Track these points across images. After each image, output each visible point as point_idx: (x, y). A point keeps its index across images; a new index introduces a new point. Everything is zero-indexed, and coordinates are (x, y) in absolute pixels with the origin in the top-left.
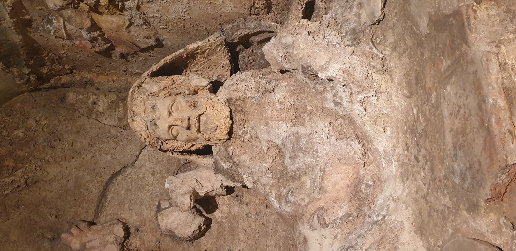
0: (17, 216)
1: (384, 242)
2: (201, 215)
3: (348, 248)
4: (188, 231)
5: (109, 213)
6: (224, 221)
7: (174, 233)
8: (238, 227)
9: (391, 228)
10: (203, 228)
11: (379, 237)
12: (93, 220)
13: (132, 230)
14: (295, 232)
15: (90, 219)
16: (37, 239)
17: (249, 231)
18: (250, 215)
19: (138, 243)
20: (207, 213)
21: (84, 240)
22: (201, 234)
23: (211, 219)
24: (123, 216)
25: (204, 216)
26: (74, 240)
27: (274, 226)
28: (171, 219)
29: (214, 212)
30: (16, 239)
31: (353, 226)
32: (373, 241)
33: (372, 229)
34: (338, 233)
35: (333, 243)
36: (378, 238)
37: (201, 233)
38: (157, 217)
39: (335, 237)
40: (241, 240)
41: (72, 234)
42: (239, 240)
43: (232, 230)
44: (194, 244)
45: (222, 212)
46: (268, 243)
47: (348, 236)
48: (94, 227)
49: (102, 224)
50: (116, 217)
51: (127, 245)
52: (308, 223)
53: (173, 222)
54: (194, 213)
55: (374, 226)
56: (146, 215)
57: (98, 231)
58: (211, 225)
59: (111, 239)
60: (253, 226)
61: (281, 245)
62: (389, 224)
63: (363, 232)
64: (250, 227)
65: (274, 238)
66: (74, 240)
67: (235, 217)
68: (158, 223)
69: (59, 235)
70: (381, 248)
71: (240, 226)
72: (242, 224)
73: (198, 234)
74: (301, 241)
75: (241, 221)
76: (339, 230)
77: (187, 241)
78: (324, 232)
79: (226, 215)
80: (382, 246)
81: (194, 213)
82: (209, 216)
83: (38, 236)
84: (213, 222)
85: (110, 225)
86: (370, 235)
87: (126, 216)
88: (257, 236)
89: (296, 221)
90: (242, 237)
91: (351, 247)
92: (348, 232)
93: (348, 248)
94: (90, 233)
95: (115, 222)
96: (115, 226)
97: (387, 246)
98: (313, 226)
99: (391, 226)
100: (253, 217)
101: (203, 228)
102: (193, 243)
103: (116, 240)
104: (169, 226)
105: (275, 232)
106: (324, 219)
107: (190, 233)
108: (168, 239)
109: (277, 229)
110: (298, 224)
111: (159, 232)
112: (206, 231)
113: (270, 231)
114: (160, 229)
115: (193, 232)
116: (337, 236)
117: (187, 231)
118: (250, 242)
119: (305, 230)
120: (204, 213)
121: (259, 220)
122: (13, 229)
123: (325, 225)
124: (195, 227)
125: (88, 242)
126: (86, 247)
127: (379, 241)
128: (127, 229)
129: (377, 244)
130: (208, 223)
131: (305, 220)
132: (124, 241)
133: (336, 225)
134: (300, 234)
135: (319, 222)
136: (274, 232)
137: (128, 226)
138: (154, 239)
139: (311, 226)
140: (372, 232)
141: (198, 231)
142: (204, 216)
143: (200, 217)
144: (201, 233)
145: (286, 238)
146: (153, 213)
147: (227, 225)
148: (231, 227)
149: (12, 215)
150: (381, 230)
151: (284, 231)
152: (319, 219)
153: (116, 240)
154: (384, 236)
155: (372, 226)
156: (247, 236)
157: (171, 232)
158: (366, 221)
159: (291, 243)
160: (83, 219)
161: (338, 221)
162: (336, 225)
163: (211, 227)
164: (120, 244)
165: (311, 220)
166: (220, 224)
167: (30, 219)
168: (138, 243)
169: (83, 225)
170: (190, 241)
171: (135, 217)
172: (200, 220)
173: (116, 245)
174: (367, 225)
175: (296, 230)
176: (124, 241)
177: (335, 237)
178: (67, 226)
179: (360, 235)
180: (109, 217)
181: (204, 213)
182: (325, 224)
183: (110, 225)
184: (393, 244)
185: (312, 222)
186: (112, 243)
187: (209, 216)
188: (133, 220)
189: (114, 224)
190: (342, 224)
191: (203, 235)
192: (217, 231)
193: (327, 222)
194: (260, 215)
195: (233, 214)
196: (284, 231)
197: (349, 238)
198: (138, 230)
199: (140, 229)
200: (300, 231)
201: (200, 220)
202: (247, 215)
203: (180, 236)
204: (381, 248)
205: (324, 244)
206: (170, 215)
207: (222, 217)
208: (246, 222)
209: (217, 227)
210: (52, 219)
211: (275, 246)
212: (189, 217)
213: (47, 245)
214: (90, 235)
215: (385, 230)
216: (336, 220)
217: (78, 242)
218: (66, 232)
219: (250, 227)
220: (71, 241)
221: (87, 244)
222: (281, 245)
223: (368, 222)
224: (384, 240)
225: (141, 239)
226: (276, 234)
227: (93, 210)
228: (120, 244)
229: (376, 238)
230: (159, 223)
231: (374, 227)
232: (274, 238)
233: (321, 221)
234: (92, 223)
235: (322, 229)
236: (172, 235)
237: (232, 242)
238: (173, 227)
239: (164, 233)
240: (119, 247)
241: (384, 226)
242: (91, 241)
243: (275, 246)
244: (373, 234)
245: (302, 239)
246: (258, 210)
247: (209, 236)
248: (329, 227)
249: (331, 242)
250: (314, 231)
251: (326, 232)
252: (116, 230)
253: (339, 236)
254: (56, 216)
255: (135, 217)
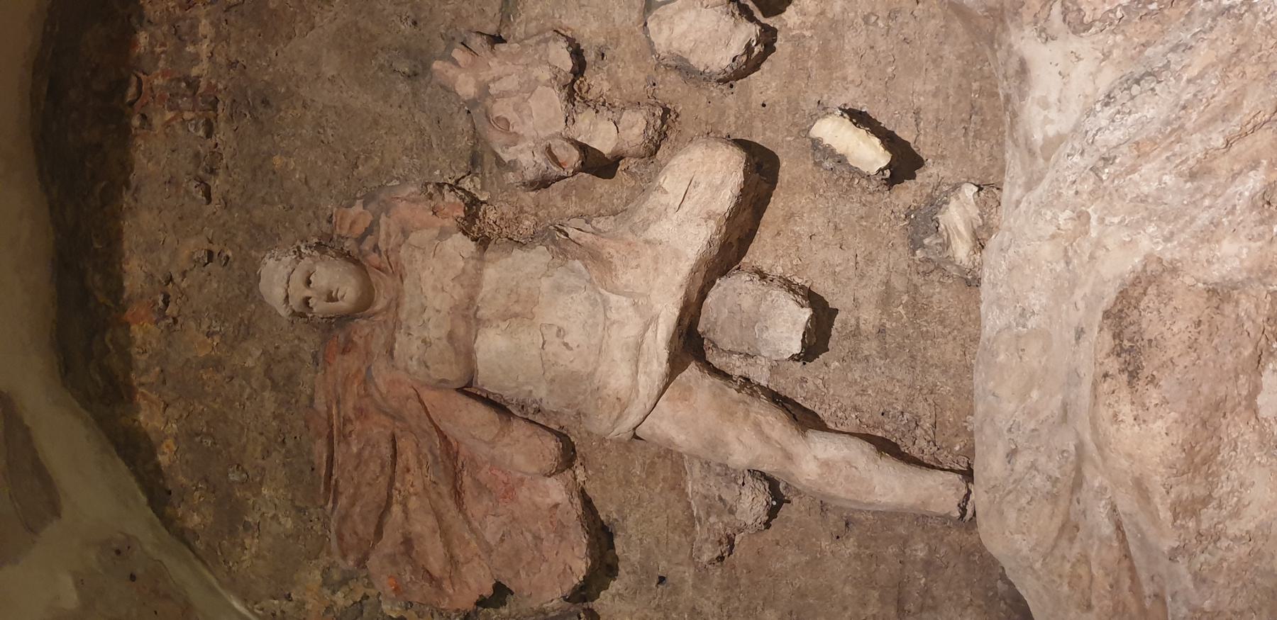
0: (330, 22)
1: (1242, 60)
2: (751, 18)
3: (1142, 77)
4: (722, 58)
5: (533, 15)
6: (808, 34)
7: (687, 61)
8: (843, 48)
9: (1269, 22)
10: (756, 50)
11: (1231, 49)
12: (499, 31)
13: (590, 57)
14: (994, 51)
15: (491, 29)
16: (381, 74)
17: (869, 58)
18: (873, 19)
19: (606, 86)
20: (765, 16)
21: (485, 76)
22: (751, 64)
23: (773, 32)
24: (565, 22)
25: (758, 22)
26: (462, 77)
27: (936, 46)
28: (681, 27)
29: (783, 11)
30: (335, 73)
31: (1157, 27)
32: (1212, 58)
33: (1211, 28)
34: (1115, 45)
35: (1100, 70)
36: (1227, 49)
37: (750, 63)
38: (646, 24)
39: (1106, 56)
40: (849, 79)
41: (455, 62)
42: (845, 79)
43: (828, 58)
44: (736, 89)
45: (803, 13)
46: (918, 86)
47: (1141, 52)
48: (502, 48)
49: (520, 41)
50: (549, 25)
51: (580, 89)
52: (1036, 24)
53: (684, 35)
54: (733, 15)
55: (1221, 20)
56: (618, 21)
57: (513, 57)
58: (776, 45)
59: (545, 74)
60: (882, 45)
61: (951, 92)
62: (1265, 14)
63: (1186, 37)
64: (872, 48)
65: (933, 74)
66: (462, 77)
67: (834, 25)
68: (649, 39)
69: (427, 67)
70: (1231, 75)
71: (847, 47)
72: (854, 40)
73: (746, 63)
74: (1011, 72)
75: (850, 35)
76: (1119, 38)
77: (719, 81)
78: (1075, 44)
79: (812, 19)
80: (1237, 70)
81: (733, 15)
82: (771, 22)
83: (381, 67)
84: (779, 36)
85: (538, 43)
86: (1205, 44)
87: (573, 22)
88: (890, 70)
89: (1002, 21)
90: (851, 71)
91: (1150, 74)
92: (1143, 40)
93: (1142, 77)
94: (496, 60)
95: (547, 35)
96: (551, 44)
97: (1249, 70)
98: (1049, 31)
99: (1269, 17)
100: (881, 24)
101: (756, 50)
102: (732, 86)
103: (555, 78)
104: (675, 45)
105: (937, 60)
106: (1080, 10)
107: (728, 62)
108: (673, 76)
109: (941, 53)
110: (1005, 29)
111: (652, 60)
112: (763, 57)
113: (924, 57)
114: (653, 52)
115: (734, 60)
116: (1110, 52)
117: (718, 57)
118: (871, 84)
119: (1025, 42)
120: (758, 15)
121: (895, 32)
122: (325, 51)
123: (1079, 27)
124: (737, 48)
125: (494, 80)
126: (491, 91)
127: (1230, 59)
128: (577, 54)
129: (1221, 66)
130: (768, 38)
131: (1027, 17)
132: (573, 81)
133: (1111, 24)
134: (1010, 52)
135: (1064, 20)
136: (934, 61)
137: (578, 45)
138: (642, 77)
139: (1044, 30)
140: (1213, 36)
141: (744, 58)
142: (758, 22)
143: (750, 24)
144: (750, 63)
145: (964, 74)
146: (635, 16)
147: (815, 45)
148: (824, 48)
149: (317, 19)
150: (1237, 30)
151: (960, 57)
152: (1065, 13)
153: (555, 78)
154: (1244, 45)
155: (1214, 20)
156: (863, 71)
157: (682, 59)
158: (1198, 10)
159: (975, 86)
160: (475, 29)
161: (1119, 14)
162: (1111, 24)
163: (774, 50)
164: (564, 87)
165: (1043, 15)
166: (798, 40)
167: (358, 30)
168: (606, 86)
169: (476, 42)
170: (724, 81)
171: (594, 26)
172: (748, 32)
173: (557, 88)
174: (1198, 20)
175: (1000, 45)
176: (573, 81)
177: (1106, 56)
178: (442, 45)
179: (1177, 46)
180: (534, 23)
181: (758, 15)
182: (1082, 22)
183: (538, 43)
184: (1267, 64)
185: (1046, 20)
186: (548, 84)
187: (771, 22)
188: (589, 32)
189: (546, 41)
190: (1129, 22)
191: (756, 67)
192: (791, 58)
193: (1087, 19)
194: (900, 20)
195: (830, 15)
196: (960, 57)
197: (1146, 53)
198: (603, 55)
199: (608, 54)
200: (1011, 46)
201: (748, 32)
202: (866, 19)
203: (702, 69)
204: (1231, 75)
205: (1073, 75)
206: (676, 18)
207: (802, 25)
208: (864, 37)
209: (789, 49)
210: (406, 28)
211: (935, 95)
212: (722, 23)
213: (404, 87)
214: (495, 66)
215: (1251, 29)
216: (1113, 11)
217: (472, 81)
218: (440, 59)
219: (872, 48)
220: (455, 78)
221: (491, 85)
222: (951, 92)
223: (1203, 12)
224: (1243, 55)
225: (610, 76)
226: (938, 66)
227: (497, 8)
228: (564, 87)
229: (1222, 52)
230: (653, 39)
231: (1220, 23)
232: (933, 74)
233: (1072, 16)
234: (496, 39)
235: (1072, 37)
236: (683, 68)
237: (827, 86)
238: (686, 47)
239: (664, 62)
240: (564, 94)
241: (1248, 18)
242: (500, 78)
243: (935, 95)
244: (1214, 41)
245: (1014, 65)
246: (894, 6)
247: (770, 71)
248: (1093, 30)
249: (1093, 70)
250: (1051, 44)
251: (1082, 44)
252: (552, 53)
253: (1116, 53)
254: (415, 23)
255: (594, 26)
